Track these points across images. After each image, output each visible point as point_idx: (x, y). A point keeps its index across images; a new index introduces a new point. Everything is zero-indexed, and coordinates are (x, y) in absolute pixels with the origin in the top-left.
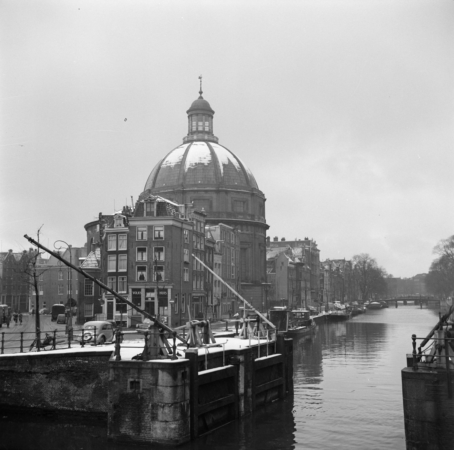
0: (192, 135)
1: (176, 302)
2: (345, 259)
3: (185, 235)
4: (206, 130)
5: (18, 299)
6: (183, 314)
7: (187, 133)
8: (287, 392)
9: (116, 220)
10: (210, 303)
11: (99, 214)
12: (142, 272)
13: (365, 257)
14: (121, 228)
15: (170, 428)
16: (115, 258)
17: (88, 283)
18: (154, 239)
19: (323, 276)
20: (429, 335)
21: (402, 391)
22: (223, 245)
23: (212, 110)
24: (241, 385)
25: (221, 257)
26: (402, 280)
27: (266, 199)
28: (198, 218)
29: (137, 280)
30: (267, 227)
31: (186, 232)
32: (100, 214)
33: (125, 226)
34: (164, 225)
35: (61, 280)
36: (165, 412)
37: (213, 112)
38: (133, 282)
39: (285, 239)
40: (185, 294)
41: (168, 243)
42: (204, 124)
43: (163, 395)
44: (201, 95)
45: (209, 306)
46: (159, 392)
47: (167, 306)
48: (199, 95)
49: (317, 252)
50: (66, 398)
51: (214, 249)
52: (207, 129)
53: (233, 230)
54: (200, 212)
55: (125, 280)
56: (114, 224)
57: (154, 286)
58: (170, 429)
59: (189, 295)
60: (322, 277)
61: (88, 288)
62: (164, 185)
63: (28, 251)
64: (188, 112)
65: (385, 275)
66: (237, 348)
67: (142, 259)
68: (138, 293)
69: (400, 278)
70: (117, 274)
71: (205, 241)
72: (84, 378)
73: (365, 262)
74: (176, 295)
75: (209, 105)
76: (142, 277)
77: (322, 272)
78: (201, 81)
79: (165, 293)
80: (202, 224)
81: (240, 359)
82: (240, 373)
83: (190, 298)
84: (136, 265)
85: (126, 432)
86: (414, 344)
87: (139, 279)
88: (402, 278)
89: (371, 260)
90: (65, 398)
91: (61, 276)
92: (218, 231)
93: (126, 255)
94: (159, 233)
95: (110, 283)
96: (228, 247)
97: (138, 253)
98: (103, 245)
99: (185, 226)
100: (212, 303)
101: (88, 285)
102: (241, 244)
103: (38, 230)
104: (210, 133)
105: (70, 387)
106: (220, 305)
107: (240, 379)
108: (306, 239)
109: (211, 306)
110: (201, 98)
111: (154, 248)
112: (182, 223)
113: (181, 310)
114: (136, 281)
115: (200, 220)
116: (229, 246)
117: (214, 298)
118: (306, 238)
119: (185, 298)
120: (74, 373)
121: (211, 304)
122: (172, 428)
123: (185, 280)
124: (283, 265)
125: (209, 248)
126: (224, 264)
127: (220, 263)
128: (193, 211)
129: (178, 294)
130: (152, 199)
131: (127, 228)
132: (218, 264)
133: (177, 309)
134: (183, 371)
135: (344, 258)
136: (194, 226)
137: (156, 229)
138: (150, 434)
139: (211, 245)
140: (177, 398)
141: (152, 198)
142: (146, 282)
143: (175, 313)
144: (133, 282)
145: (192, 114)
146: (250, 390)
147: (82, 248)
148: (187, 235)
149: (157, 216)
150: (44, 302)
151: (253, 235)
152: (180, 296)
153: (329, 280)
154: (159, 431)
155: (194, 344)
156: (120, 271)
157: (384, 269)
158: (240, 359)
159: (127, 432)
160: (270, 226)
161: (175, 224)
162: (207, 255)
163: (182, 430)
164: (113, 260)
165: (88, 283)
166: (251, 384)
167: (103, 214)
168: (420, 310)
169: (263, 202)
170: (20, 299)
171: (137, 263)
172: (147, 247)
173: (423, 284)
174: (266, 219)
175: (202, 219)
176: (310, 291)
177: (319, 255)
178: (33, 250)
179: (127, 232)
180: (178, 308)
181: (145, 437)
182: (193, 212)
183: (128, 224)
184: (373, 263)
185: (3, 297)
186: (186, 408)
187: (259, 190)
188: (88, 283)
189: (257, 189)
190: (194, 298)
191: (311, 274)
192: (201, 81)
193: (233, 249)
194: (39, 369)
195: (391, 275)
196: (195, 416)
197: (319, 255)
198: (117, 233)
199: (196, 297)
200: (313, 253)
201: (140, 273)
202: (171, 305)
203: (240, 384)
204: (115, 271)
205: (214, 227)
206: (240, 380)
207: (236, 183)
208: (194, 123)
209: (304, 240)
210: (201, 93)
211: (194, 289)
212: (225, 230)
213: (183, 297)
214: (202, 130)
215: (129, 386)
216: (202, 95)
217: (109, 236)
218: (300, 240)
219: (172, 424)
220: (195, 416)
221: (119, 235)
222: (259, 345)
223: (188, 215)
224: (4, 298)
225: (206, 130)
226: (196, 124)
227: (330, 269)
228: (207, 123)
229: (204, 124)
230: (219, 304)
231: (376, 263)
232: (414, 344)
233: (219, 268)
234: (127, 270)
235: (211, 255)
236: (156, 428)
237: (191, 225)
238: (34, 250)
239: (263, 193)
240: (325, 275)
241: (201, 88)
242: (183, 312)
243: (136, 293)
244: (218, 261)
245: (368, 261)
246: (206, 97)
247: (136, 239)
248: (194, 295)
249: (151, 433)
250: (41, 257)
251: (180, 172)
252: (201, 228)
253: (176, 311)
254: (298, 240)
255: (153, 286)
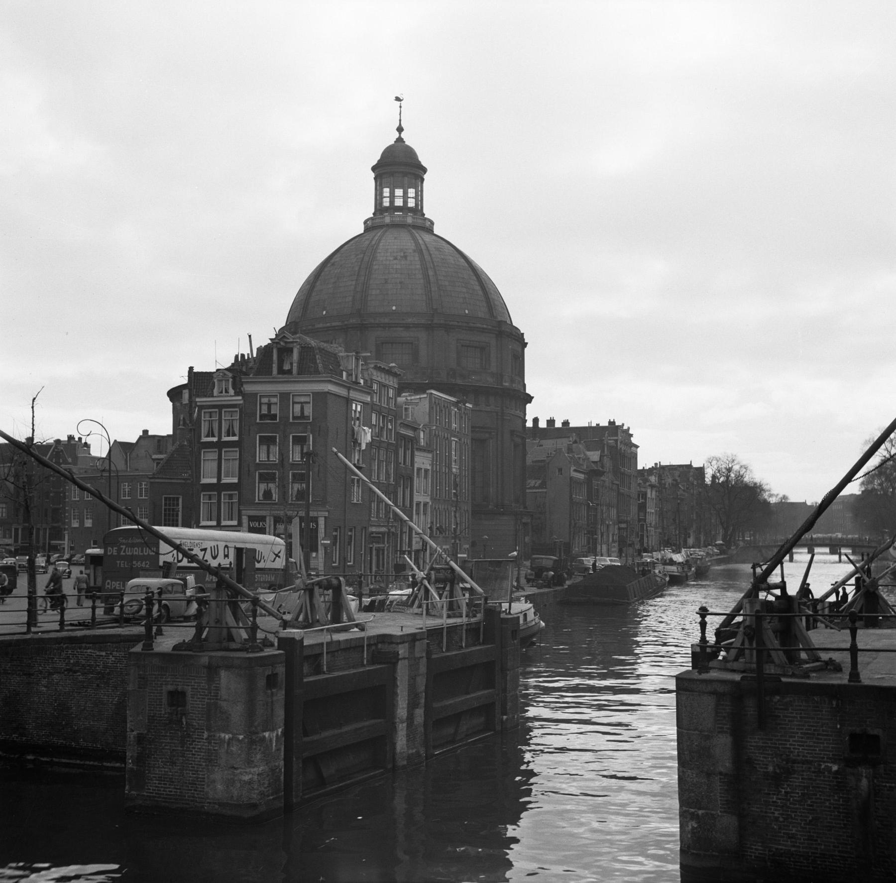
0: (382, 214)
1: (334, 543)
2: (692, 464)
3: (355, 411)
4: (409, 206)
5: (45, 533)
6: (349, 566)
7: (373, 211)
8: (505, 717)
9: (219, 381)
10: (407, 547)
11: (188, 369)
12: (267, 483)
13: (729, 459)
14: (228, 396)
15: (240, 781)
16: (215, 456)
17: (169, 504)
18: (293, 420)
19: (644, 495)
20: (735, 607)
21: (676, 718)
22: (435, 432)
23: (422, 166)
24: (400, 703)
25: (430, 455)
26: (810, 506)
27: (527, 343)
28: (378, 377)
29: (259, 500)
30: (529, 399)
31: (357, 407)
32: (191, 368)
33: (235, 393)
34: (312, 393)
35: (127, 498)
36: (232, 751)
37: (424, 170)
38: (252, 503)
39: (569, 423)
40: (355, 527)
41: (320, 427)
42: (405, 194)
43: (228, 718)
44: (400, 134)
45: (405, 551)
46: (220, 711)
47: (317, 551)
48: (397, 135)
49: (633, 448)
50: (64, 723)
51: (416, 440)
52: (411, 203)
53: (456, 404)
54: (387, 368)
55: (235, 500)
56: (214, 388)
57: (279, 512)
58: (240, 783)
59: (362, 529)
60: (642, 498)
61: (169, 514)
62: (324, 313)
63: (65, 441)
64: (374, 169)
65: (771, 496)
66: (396, 631)
67: (268, 457)
68: (259, 525)
69: (805, 503)
70: (219, 487)
71: (398, 425)
72: (98, 685)
73: (729, 470)
74: (336, 530)
75: (417, 156)
76: (268, 494)
77: (643, 490)
78: (400, 107)
79: (313, 526)
80: (391, 393)
81: (398, 652)
82: (398, 678)
83: (365, 535)
84: (256, 471)
85: (159, 787)
86: (703, 625)
87: (261, 498)
88: (809, 503)
89: (741, 467)
90: (62, 723)
91: (127, 490)
92: (425, 406)
93: (237, 449)
94: (302, 409)
95: (206, 506)
96: (444, 437)
97: (261, 446)
98: (194, 430)
99: (353, 394)
100: (410, 545)
101: (169, 510)
102: (472, 431)
103: (32, 399)
104: (418, 210)
105: (71, 701)
106: (426, 550)
107: (399, 691)
108: (610, 423)
109: (408, 551)
110: (400, 140)
111: (291, 438)
112: (349, 389)
113: (345, 559)
114: (257, 501)
115: (387, 382)
116: (448, 435)
117: (414, 535)
118: (612, 420)
119: (340, 535)
120: (80, 675)
121: (409, 547)
122: (245, 781)
123: (355, 501)
124: (561, 474)
125: (404, 437)
126: (445, 471)
127: (429, 468)
128: (373, 366)
129: (340, 527)
130: (288, 341)
131: (240, 398)
132: (423, 470)
133: (336, 556)
134: (268, 672)
135: (691, 462)
136: (375, 395)
137: (297, 399)
138: (203, 791)
139: (410, 433)
140: (256, 724)
141: (288, 339)
142: (276, 504)
143: (333, 565)
144: (252, 503)
145: (381, 172)
146: (419, 713)
147: (168, 436)
148: (360, 412)
149: (298, 374)
150: (94, 541)
151: (500, 414)
152: (342, 531)
153: (656, 504)
154: (219, 787)
155: (311, 622)
156: (225, 480)
157: (767, 484)
158: (400, 653)
159: (162, 787)
160: (533, 397)
161: (332, 389)
162: (401, 452)
163: (266, 786)
164: (211, 460)
165: (170, 506)
166: (423, 701)
167: (195, 370)
168: (838, 565)
169: (520, 349)
170: (49, 534)
171: (259, 466)
172: (278, 435)
173: (849, 515)
174: (526, 382)
175: (392, 382)
176: (617, 526)
177: (636, 454)
178: (74, 438)
179: (239, 404)
180: (339, 554)
181: (193, 797)
182: (372, 368)
183: (242, 389)
184: (746, 472)
185: (16, 530)
186: (274, 744)
187: (514, 324)
188: (169, 504)
189: (509, 322)
190: (372, 535)
191: (619, 494)
192: (400, 107)
193: (456, 441)
194: (14, 665)
195: (784, 497)
196: (294, 759)
197: (636, 454)
198: (220, 407)
199: (376, 534)
200: (624, 450)
201: (263, 486)
202: (323, 549)
203: (398, 701)
204: (214, 481)
205: (418, 397)
206: (397, 693)
207: (467, 312)
208: (386, 192)
209: (607, 424)
210: (400, 129)
211: (372, 519)
212: (439, 404)
213: (350, 533)
214: (402, 205)
215: (165, 701)
216: (403, 135)
217: (225, 412)
218: (598, 425)
219: (244, 774)
220: (294, 759)
221: (224, 410)
222: (445, 626)
223: (362, 373)
224: (18, 532)
225: (409, 206)
226: (390, 193)
227: (660, 483)
228: (411, 192)
229: (405, 194)
230: (424, 548)
231: (751, 471)
232: (703, 625)
233: (426, 478)
234: (239, 479)
235: (409, 453)
236: (214, 781)
237: (369, 393)
238: (77, 439)
239: (522, 332)
240: (649, 495)
241: (400, 120)
242: (348, 564)
243: (257, 524)
244: (423, 463)
245: (736, 468)
246: (409, 139)
247: (256, 419)
248: (374, 529)
249: (205, 790)
250: (91, 453)
251: (355, 288)
252: (389, 398)
253: (334, 560)
254: (594, 425)
255: (276, 512)
